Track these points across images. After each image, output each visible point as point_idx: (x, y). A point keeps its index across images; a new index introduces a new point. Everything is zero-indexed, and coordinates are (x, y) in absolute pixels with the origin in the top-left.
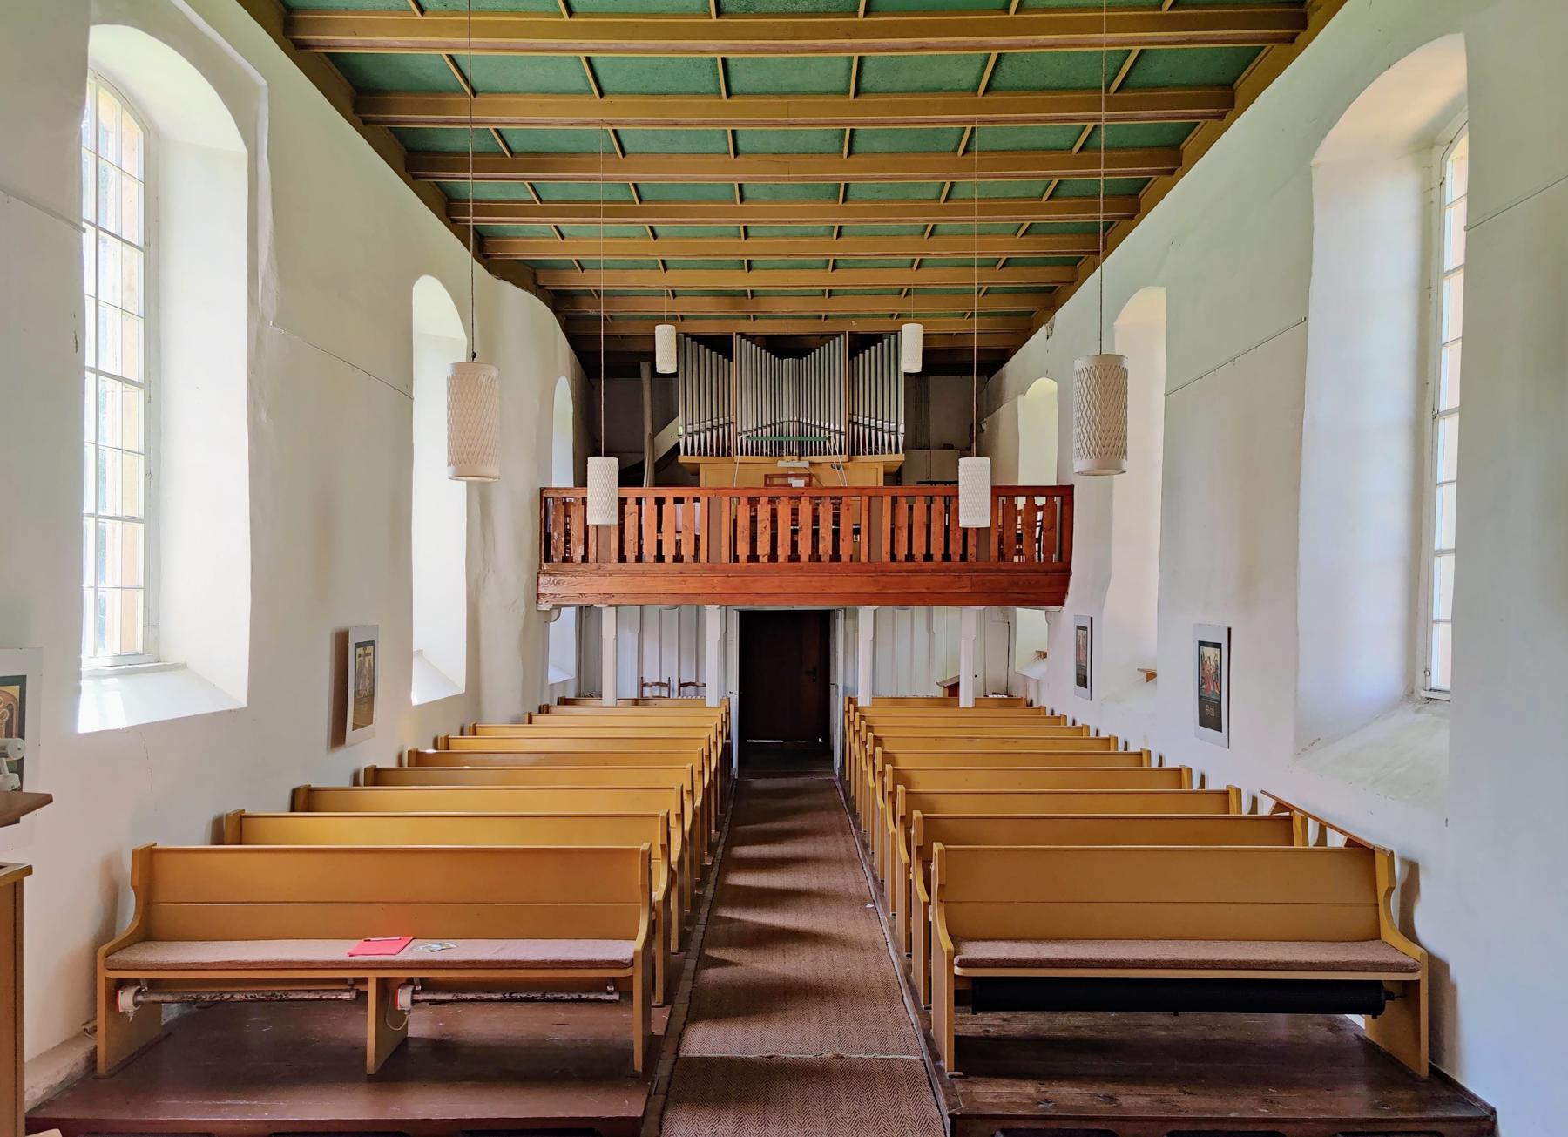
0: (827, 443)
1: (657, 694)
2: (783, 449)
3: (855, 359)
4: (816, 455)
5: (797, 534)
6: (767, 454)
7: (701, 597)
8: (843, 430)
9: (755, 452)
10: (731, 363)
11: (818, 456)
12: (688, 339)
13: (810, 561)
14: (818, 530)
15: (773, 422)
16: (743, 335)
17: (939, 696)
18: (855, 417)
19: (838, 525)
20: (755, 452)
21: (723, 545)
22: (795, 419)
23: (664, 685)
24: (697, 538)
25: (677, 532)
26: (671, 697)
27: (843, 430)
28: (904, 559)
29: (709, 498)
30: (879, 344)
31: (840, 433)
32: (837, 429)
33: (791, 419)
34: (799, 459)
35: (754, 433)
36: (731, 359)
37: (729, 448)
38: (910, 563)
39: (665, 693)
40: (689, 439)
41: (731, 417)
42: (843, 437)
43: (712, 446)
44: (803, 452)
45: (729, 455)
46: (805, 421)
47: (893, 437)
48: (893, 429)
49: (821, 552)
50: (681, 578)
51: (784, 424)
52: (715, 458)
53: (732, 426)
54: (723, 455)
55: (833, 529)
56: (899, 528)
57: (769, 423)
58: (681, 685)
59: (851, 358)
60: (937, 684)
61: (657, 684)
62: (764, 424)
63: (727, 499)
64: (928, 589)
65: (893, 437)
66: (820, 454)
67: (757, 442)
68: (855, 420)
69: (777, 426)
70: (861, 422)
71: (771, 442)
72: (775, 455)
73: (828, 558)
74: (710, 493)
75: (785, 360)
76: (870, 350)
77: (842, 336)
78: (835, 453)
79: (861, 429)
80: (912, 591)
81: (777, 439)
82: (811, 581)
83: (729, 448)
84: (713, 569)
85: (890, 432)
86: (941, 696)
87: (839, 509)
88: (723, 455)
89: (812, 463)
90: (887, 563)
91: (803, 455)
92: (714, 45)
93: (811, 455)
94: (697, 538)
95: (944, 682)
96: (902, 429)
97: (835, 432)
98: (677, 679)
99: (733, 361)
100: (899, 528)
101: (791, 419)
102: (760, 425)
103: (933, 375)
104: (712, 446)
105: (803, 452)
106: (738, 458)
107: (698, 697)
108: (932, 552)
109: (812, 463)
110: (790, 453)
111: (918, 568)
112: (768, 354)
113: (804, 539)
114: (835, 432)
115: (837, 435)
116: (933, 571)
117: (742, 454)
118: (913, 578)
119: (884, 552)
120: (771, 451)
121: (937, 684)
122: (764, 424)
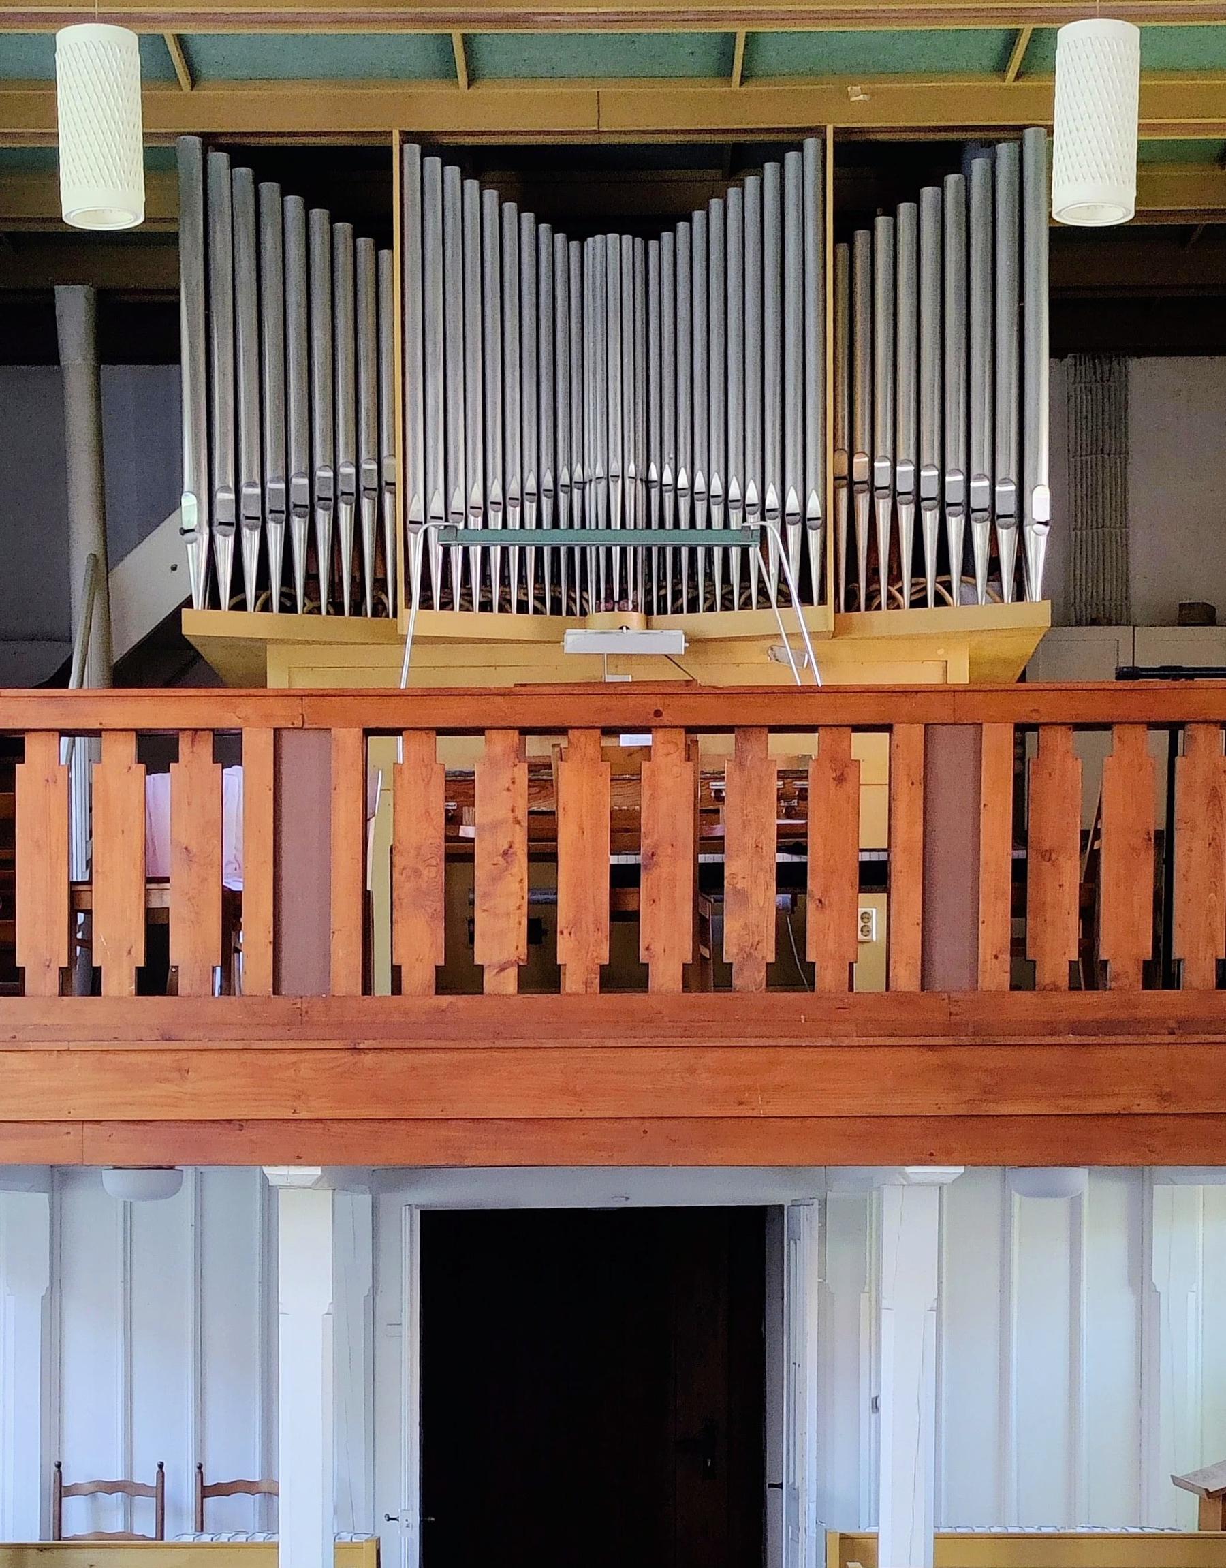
0: (754, 553)
1: (119, 1527)
2: (584, 588)
3: (861, 236)
4: (711, 609)
5: (636, 883)
6: (522, 607)
7: (246, 1134)
8: (814, 508)
9: (477, 598)
10: (384, 253)
11: (718, 613)
12: (220, 160)
13: (686, 987)
14: (720, 867)
15: (548, 482)
16: (429, 144)
17: (1185, 1531)
18: (861, 461)
19: (801, 849)
20: (477, 598)
21: (336, 924)
22: (631, 470)
23: (140, 1490)
24: (232, 904)
25: (149, 880)
26: (169, 1538)
27: (814, 508)
28: (1064, 982)
29: (277, 732)
30: (951, 179)
31: (804, 520)
32: (793, 504)
33: (615, 468)
34: (648, 626)
35: (476, 522)
36: (384, 242)
37: (380, 584)
38: (1093, 997)
39: (145, 1525)
40: (225, 547)
41: (386, 462)
42: (814, 538)
43: (312, 578)
44: (662, 599)
45: (379, 609)
46: (668, 478)
47: (1006, 538)
48: (1007, 506)
49: (730, 953)
50: (166, 1059)
51: (590, 490)
52: (325, 624)
53: (387, 498)
54: (357, 610)
55: (780, 866)
56: (1047, 855)
57: (531, 486)
58: (206, 1492)
59: (844, 235)
60: (1176, 1481)
61: (112, 1488)
62: (514, 488)
63: (349, 737)
64: (1164, 1097)
65: (1006, 538)
66: (727, 605)
67: (485, 552)
68: (860, 473)
69: (563, 498)
70: (882, 480)
71: (539, 552)
72: (556, 610)
73: (761, 976)
74: (282, 714)
75: (595, 243)
76: (917, 200)
77: (811, 144)
78: (785, 598)
79: (883, 508)
80: (1096, 1107)
81: (563, 537)
82: (692, 1071)
83: (380, 584)
84: (299, 1021)
85: (994, 518)
86: (1194, 1530)
87: (804, 815)
88: (357, 610)
89: (695, 642)
90: (1000, 994)
91: (662, 611)
92: (577, 409)
93: (693, 607)
94: (232, 904)
95: (1203, 1473)
96: (1040, 504)
97: (784, 517)
98: (192, 1470)
99: (390, 247)
100: (1047, 855)
101: (615, 468)
102: (495, 493)
103: (1141, 353)
104: (312, 578)
105: (662, 599)
106: (413, 620)
107: (206, 1538)
108: (1176, 954)
109: (695, 642)
110: (611, 602)
111: (1121, 1014)
112: (528, 217)
113: (663, 902)
114: (784, 517)
115: (794, 532)
116: (1184, 1026)
117: (426, 603)
118: (1101, 1054)
119: (986, 952)
120: (540, 599)
121: (1176, 1481)
122: (514, 488)
